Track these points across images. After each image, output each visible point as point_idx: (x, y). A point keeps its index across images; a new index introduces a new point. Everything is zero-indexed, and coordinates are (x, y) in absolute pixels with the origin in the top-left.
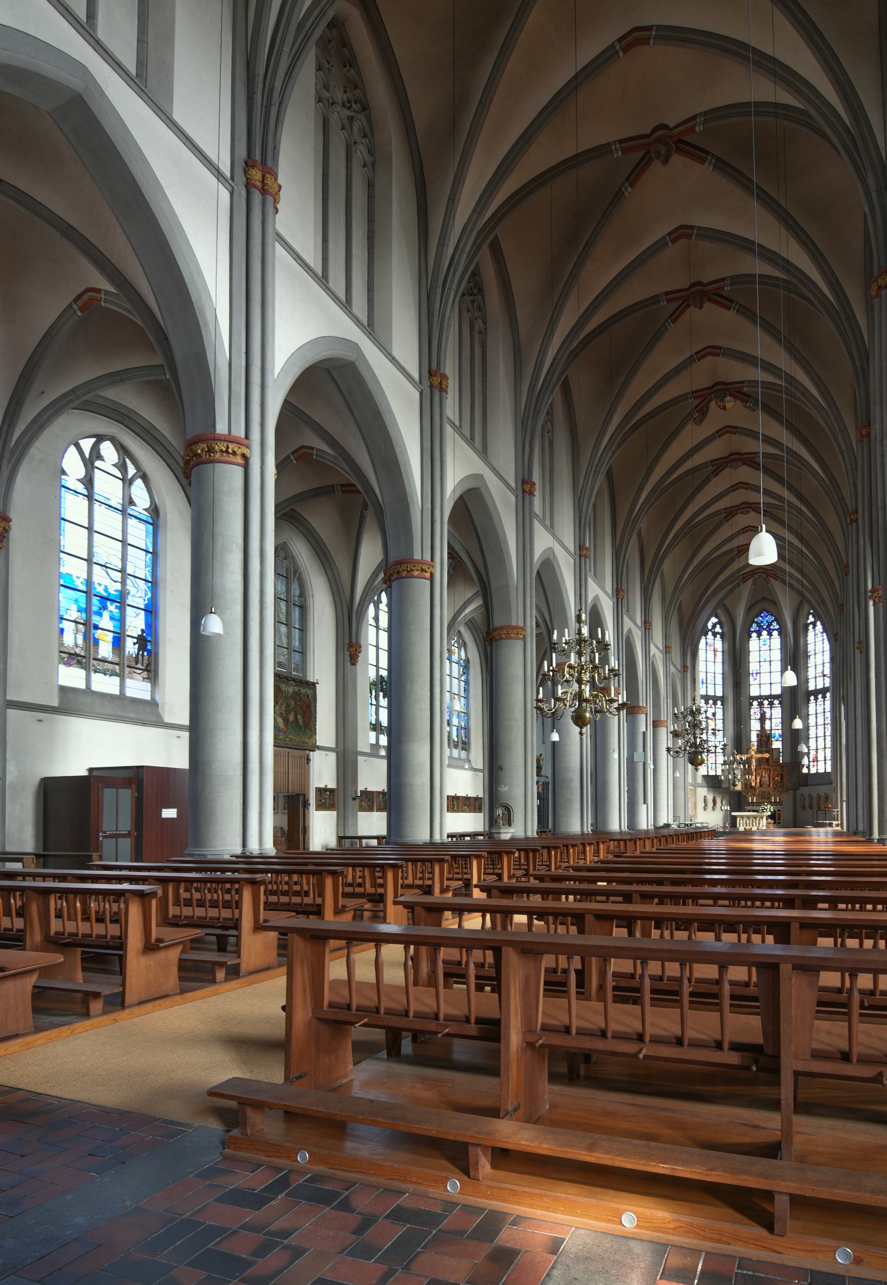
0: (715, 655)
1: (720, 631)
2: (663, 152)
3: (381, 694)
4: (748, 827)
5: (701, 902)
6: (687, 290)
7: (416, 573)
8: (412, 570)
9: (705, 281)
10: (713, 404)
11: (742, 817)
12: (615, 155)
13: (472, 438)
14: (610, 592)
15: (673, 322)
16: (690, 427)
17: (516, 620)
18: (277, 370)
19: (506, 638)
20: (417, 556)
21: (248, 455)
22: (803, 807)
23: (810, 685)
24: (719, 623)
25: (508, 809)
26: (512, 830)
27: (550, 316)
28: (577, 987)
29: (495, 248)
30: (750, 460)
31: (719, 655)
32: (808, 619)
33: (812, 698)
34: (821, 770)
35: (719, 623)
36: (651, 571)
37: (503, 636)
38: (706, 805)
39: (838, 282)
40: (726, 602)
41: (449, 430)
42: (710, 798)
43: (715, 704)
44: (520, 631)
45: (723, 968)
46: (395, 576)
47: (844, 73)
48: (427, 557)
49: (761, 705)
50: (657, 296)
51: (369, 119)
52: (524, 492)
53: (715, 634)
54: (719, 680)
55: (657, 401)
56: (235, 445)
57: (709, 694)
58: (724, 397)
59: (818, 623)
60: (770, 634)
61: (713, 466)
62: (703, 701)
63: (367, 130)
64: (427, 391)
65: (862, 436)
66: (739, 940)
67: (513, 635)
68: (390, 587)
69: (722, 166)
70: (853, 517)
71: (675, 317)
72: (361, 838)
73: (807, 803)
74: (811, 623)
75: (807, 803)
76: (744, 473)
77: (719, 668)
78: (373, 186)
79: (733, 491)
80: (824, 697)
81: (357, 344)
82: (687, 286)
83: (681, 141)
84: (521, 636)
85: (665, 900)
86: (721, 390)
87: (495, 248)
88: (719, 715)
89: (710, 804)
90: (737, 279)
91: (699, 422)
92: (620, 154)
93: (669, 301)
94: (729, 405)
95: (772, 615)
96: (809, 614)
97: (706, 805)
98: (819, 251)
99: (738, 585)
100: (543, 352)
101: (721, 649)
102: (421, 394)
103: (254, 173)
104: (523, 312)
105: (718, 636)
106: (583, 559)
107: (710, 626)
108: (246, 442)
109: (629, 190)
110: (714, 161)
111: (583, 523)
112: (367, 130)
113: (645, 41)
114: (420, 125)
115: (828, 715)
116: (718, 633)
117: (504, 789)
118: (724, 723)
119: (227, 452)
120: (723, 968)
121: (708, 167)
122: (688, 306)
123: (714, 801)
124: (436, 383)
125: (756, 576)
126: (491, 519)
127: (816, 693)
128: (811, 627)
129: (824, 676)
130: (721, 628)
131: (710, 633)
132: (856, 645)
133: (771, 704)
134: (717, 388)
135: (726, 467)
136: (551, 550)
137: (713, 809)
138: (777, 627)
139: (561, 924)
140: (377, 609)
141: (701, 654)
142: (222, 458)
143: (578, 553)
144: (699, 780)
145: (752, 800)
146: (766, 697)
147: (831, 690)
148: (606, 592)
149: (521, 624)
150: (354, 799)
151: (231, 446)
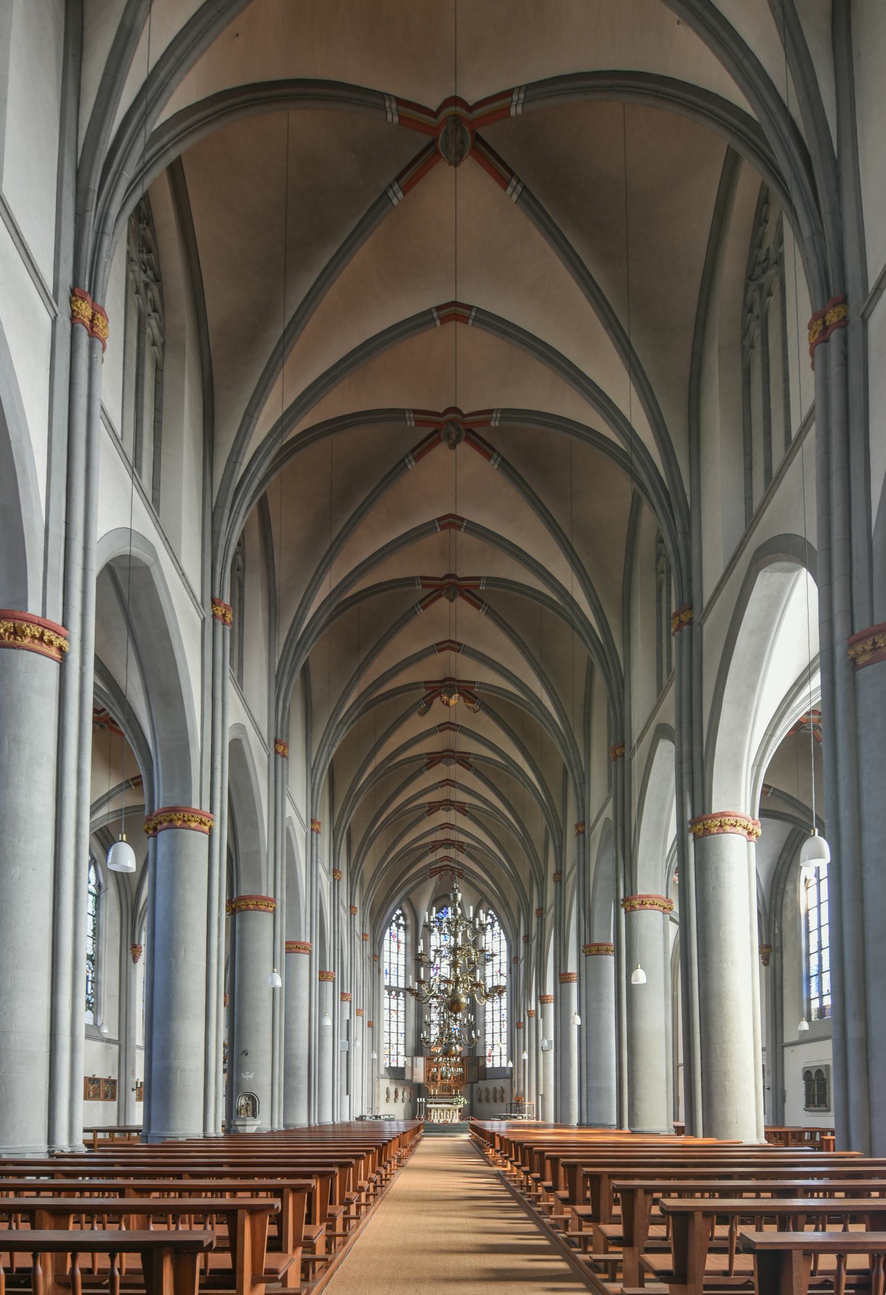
0: (398, 947)
1: (403, 923)
2: (453, 436)
5: (745, 1195)
6: (442, 579)
7: (193, 825)
8: (189, 820)
9: (459, 575)
10: (437, 701)
11: (437, 1109)
12: (409, 423)
15: (424, 608)
16: (415, 718)
17: (266, 891)
19: (254, 910)
20: (195, 805)
22: (480, 1100)
24: (403, 915)
25: (253, 1099)
26: (259, 1122)
27: (314, 571)
28: (6, 1287)
30: (464, 760)
31: (402, 946)
34: (497, 1065)
35: (403, 915)
36: (358, 855)
37: (251, 907)
38: (388, 1097)
39: (601, 607)
40: (411, 896)
42: (392, 1090)
43: (397, 995)
44: (271, 903)
45: (841, 1259)
46: (165, 824)
47: (661, 415)
48: (206, 808)
50: (413, 578)
51: (161, 291)
53: (398, 926)
54: (402, 972)
56: (52, 633)
57: (392, 985)
58: (453, 693)
61: (428, 759)
62: (386, 992)
63: (158, 304)
64: (209, 620)
65: (616, 756)
66: (169, 1229)
67: (262, 907)
68: (155, 837)
69: (506, 467)
70: (580, 828)
71: (426, 602)
73: (484, 1097)
74: (489, 924)
75: (484, 1097)
76: (456, 771)
77: (402, 961)
78: (162, 371)
79: (441, 787)
81: (154, 547)
82: (441, 576)
83: (470, 430)
84: (271, 909)
85: (184, 1194)
86: (448, 685)
88: (401, 1008)
89: (392, 1096)
90: (493, 581)
91: (423, 713)
92: (413, 424)
93: (424, 586)
94: (453, 702)
97: (388, 1097)
98: (586, 574)
99: (424, 880)
100: (304, 607)
101: (403, 941)
103: (84, 306)
104: (282, 561)
105: (402, 928)
106: (314, 833)
107: (394, 918)
108: (63, 631)
109: (413, 463)
110: (499, 460)
112: (158, 304)
113: (465, 319)
114: (213, 321)
115: (504, 1012)
116: (401, 925)
117: (248, 1076)
118: (405, 1015)
119: (41, 639)
120: (841, 1259)
121: (493, 465)
122: (440, 596)
123: (396, 1093)
124: (220, 613)
126: (248, 776)
128: (489, 927)
129: (501, 975)
130: (405, 920)
131: (394, 924)
132: (582, 948)
134: (448, 683)
135: (440, 761)
137: (395, 1101)
139: (98, 1223)
141: (386, 944)
142: (32, 645)
143: (310, 826)
144: (383, 1072)
145: (434, 1092)
147: (508, 989)
149: (271, 895)
151: (47, 633)
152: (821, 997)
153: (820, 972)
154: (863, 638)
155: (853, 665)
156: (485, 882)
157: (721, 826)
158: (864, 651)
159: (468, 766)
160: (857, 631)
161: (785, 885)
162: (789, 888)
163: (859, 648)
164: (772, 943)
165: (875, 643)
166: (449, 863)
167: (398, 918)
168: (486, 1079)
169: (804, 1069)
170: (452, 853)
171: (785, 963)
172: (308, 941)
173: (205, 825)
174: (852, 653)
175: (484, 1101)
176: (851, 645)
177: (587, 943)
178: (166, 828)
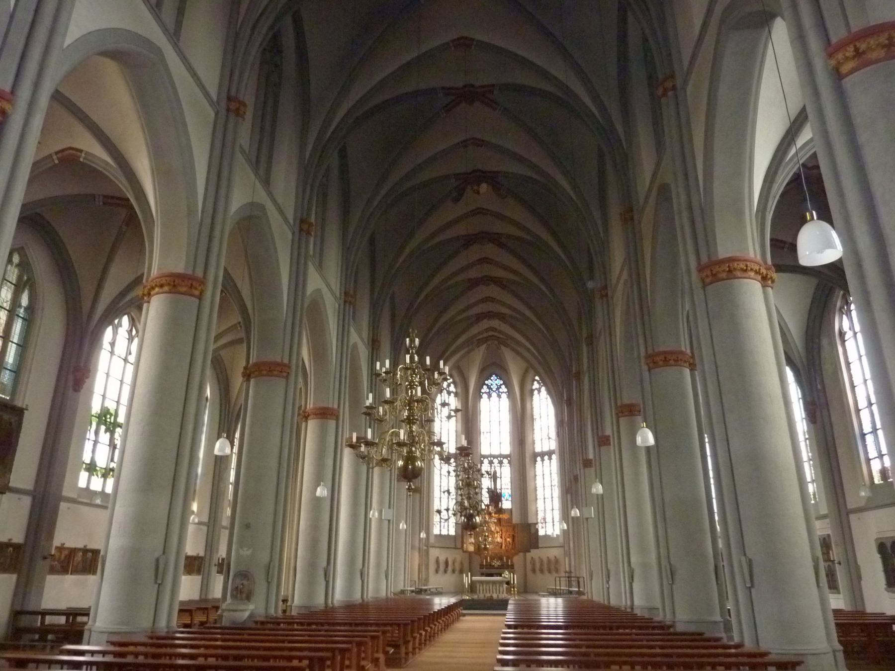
1: (454, 390)
3: (103, 428)
4: (488, 595)
13: (258, 162)
14: (366, 340)
18: (68, 41)
21: (9, 112)
22: (534, 571)
23: (536, 446)
26: (251, 607)
29: (297, 21)
30: (496, 239)
32: (533, 384)
33: (539, 459)
35: (454, 382)
38: (438, 566)
41: (239, 157)
46: (157, 290)
49: (491, 463)
52: (301, 230)
53: (449, 393)
55: (426, 175)
59: (543, 389)
60: (499, 396)
72: (44, 613)
80: (550, 459)
87: (297, 21)
89: (442, 568)
91: (456, 200)
95: (501, 379)
96: (534, 380)
102: (217, 114)
105: (452, 395)
111: (349, 273)
125: (489, 343)
127: (542, 455)
130: (456, 387)
133: (501, 463)
136: (318, 291)
137: (445, 572)
138: (506, 390)
140: (115, 333)
146: (495, 457)
147: (557, 451)
148: (362, 340)
149: (286, 361)
150: (45, 558)
152: (881, 456)
153: (874, 431)
154: (842, 45)
155: (838, 76)
156: (528, 350)
157: (730, 271)
158: (847, 59)
159: (501, 245)
160: (834, 40)
161: (820, 340)
162: (825, 342)
163: (840, 56)
164: (816, 399)
165: (856, 50)
166: (494, 333)
167: (449, 385)
168: (537, 547)
169: (876, 540)
170: (495, 323)
171: (833, 419)
172: (336, 406)
173: (196, 289)
174: (833, 62)
175: (546, 572)
176: (830, 56)
177: (619, 404)
178: (157, 293)
